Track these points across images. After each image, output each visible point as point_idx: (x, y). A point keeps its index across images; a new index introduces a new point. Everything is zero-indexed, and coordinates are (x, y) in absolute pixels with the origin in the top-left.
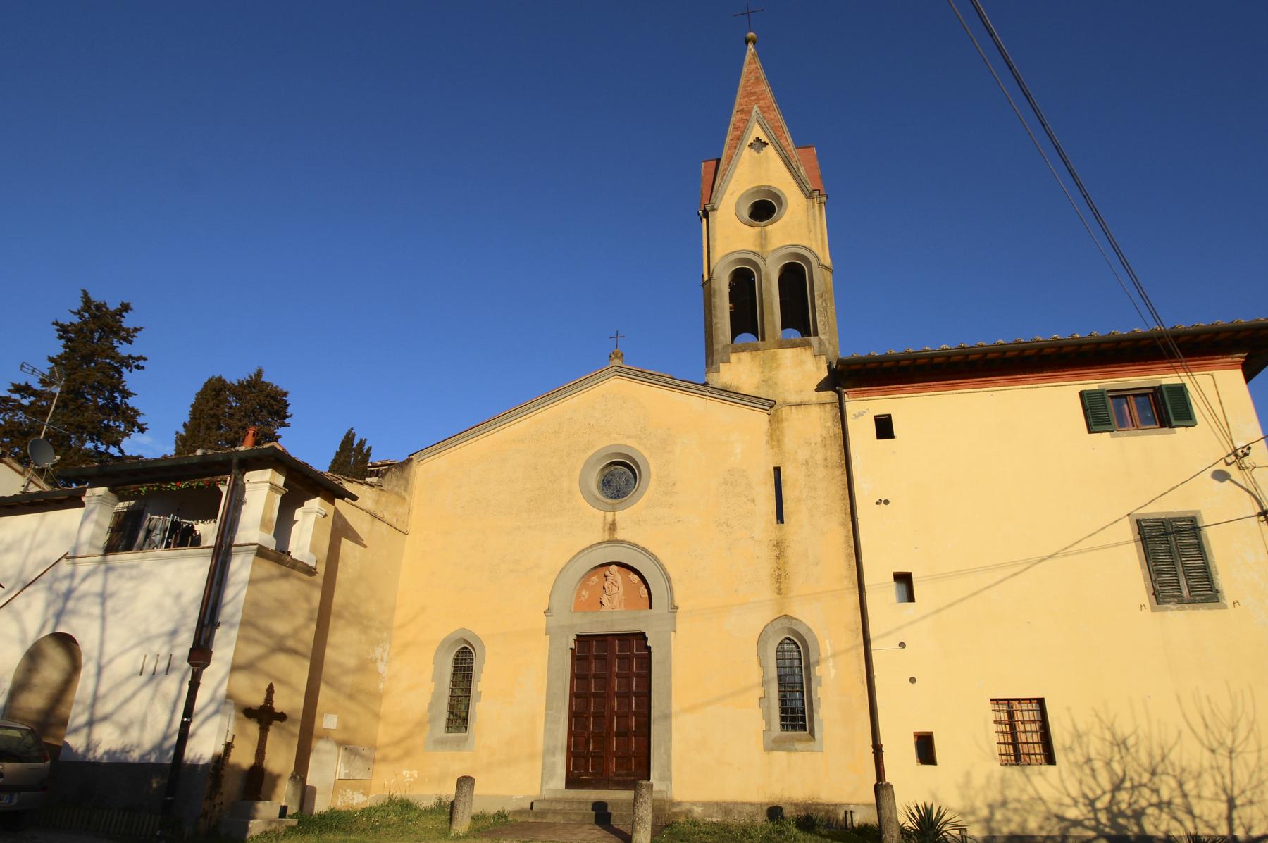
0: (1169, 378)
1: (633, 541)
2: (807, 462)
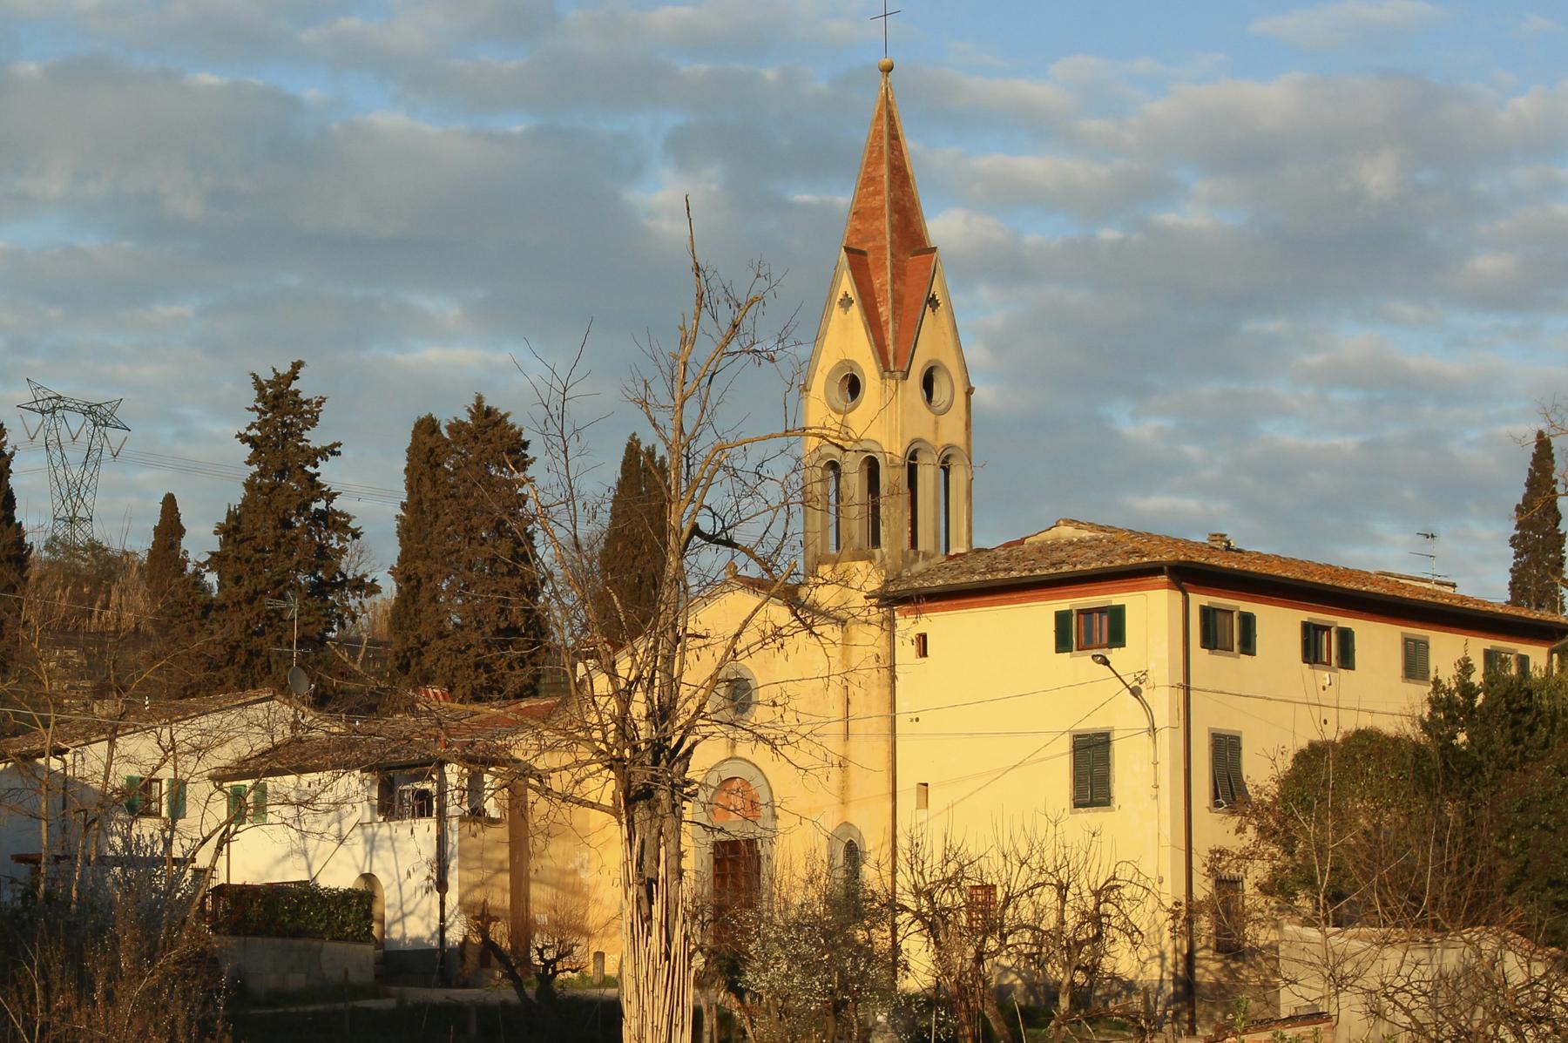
0: (1115, 599)
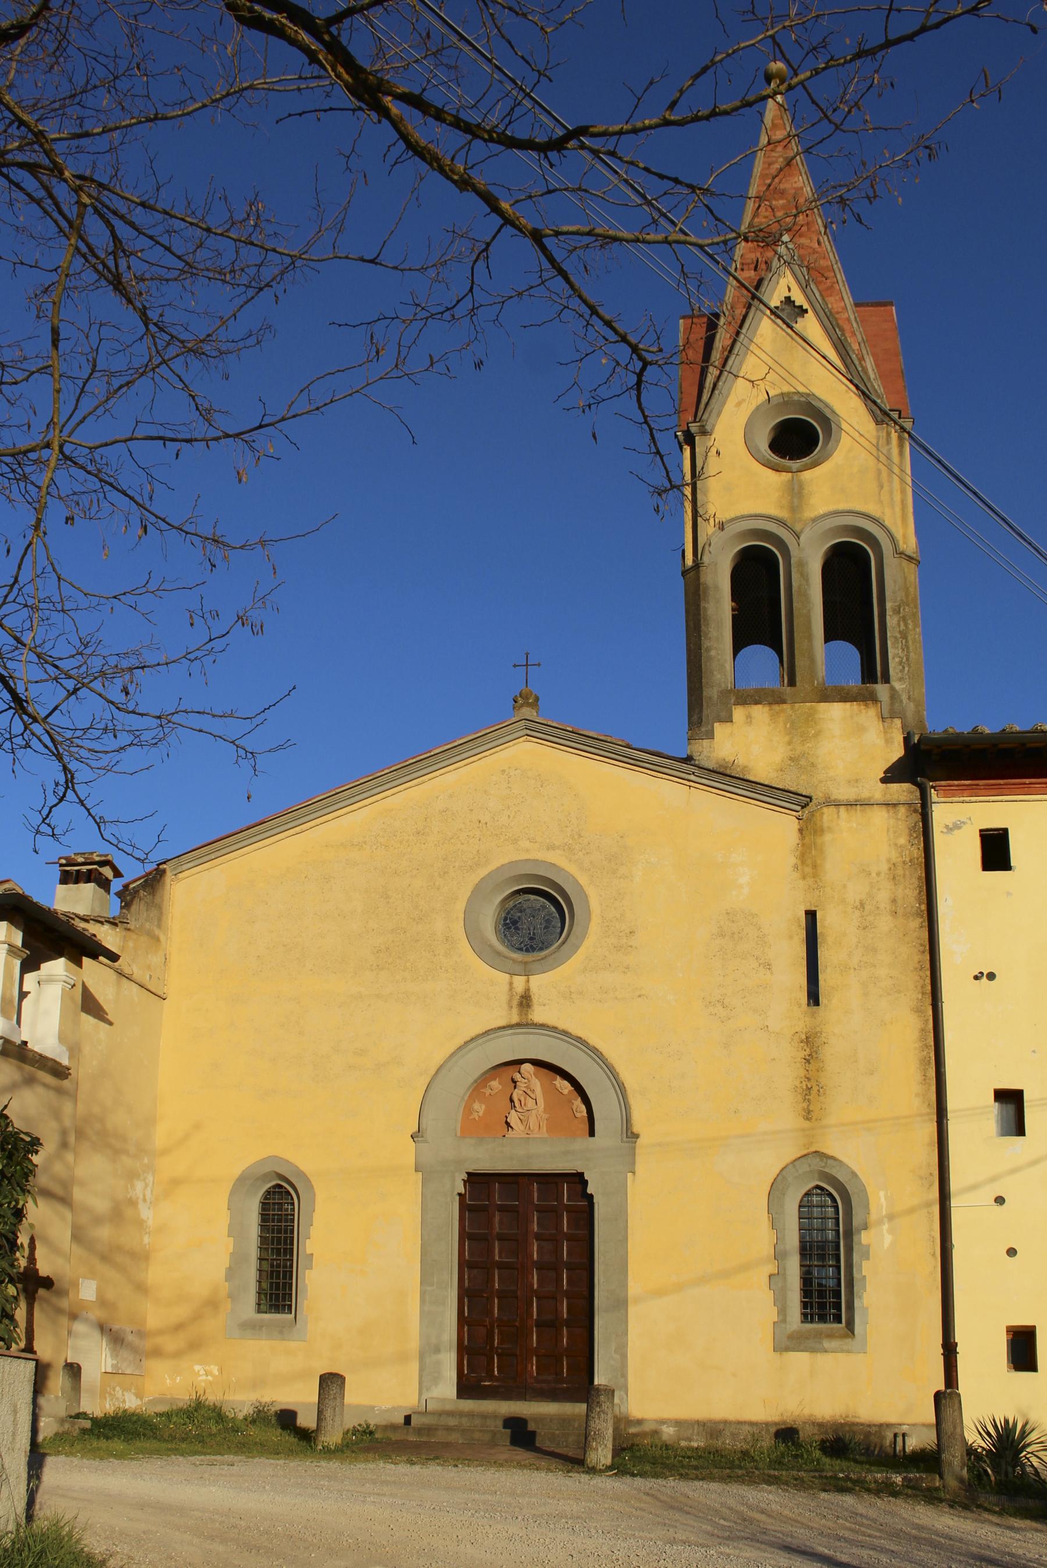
1: (561, 1026)
2: (862, 905)
